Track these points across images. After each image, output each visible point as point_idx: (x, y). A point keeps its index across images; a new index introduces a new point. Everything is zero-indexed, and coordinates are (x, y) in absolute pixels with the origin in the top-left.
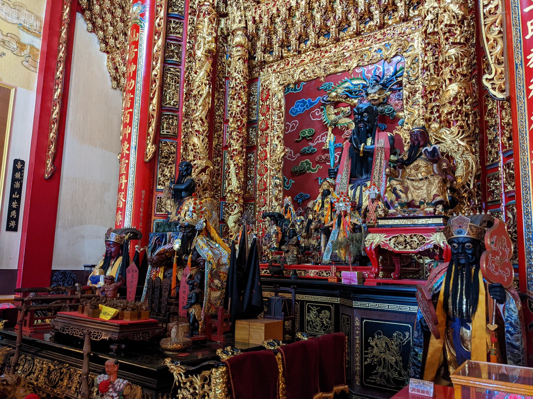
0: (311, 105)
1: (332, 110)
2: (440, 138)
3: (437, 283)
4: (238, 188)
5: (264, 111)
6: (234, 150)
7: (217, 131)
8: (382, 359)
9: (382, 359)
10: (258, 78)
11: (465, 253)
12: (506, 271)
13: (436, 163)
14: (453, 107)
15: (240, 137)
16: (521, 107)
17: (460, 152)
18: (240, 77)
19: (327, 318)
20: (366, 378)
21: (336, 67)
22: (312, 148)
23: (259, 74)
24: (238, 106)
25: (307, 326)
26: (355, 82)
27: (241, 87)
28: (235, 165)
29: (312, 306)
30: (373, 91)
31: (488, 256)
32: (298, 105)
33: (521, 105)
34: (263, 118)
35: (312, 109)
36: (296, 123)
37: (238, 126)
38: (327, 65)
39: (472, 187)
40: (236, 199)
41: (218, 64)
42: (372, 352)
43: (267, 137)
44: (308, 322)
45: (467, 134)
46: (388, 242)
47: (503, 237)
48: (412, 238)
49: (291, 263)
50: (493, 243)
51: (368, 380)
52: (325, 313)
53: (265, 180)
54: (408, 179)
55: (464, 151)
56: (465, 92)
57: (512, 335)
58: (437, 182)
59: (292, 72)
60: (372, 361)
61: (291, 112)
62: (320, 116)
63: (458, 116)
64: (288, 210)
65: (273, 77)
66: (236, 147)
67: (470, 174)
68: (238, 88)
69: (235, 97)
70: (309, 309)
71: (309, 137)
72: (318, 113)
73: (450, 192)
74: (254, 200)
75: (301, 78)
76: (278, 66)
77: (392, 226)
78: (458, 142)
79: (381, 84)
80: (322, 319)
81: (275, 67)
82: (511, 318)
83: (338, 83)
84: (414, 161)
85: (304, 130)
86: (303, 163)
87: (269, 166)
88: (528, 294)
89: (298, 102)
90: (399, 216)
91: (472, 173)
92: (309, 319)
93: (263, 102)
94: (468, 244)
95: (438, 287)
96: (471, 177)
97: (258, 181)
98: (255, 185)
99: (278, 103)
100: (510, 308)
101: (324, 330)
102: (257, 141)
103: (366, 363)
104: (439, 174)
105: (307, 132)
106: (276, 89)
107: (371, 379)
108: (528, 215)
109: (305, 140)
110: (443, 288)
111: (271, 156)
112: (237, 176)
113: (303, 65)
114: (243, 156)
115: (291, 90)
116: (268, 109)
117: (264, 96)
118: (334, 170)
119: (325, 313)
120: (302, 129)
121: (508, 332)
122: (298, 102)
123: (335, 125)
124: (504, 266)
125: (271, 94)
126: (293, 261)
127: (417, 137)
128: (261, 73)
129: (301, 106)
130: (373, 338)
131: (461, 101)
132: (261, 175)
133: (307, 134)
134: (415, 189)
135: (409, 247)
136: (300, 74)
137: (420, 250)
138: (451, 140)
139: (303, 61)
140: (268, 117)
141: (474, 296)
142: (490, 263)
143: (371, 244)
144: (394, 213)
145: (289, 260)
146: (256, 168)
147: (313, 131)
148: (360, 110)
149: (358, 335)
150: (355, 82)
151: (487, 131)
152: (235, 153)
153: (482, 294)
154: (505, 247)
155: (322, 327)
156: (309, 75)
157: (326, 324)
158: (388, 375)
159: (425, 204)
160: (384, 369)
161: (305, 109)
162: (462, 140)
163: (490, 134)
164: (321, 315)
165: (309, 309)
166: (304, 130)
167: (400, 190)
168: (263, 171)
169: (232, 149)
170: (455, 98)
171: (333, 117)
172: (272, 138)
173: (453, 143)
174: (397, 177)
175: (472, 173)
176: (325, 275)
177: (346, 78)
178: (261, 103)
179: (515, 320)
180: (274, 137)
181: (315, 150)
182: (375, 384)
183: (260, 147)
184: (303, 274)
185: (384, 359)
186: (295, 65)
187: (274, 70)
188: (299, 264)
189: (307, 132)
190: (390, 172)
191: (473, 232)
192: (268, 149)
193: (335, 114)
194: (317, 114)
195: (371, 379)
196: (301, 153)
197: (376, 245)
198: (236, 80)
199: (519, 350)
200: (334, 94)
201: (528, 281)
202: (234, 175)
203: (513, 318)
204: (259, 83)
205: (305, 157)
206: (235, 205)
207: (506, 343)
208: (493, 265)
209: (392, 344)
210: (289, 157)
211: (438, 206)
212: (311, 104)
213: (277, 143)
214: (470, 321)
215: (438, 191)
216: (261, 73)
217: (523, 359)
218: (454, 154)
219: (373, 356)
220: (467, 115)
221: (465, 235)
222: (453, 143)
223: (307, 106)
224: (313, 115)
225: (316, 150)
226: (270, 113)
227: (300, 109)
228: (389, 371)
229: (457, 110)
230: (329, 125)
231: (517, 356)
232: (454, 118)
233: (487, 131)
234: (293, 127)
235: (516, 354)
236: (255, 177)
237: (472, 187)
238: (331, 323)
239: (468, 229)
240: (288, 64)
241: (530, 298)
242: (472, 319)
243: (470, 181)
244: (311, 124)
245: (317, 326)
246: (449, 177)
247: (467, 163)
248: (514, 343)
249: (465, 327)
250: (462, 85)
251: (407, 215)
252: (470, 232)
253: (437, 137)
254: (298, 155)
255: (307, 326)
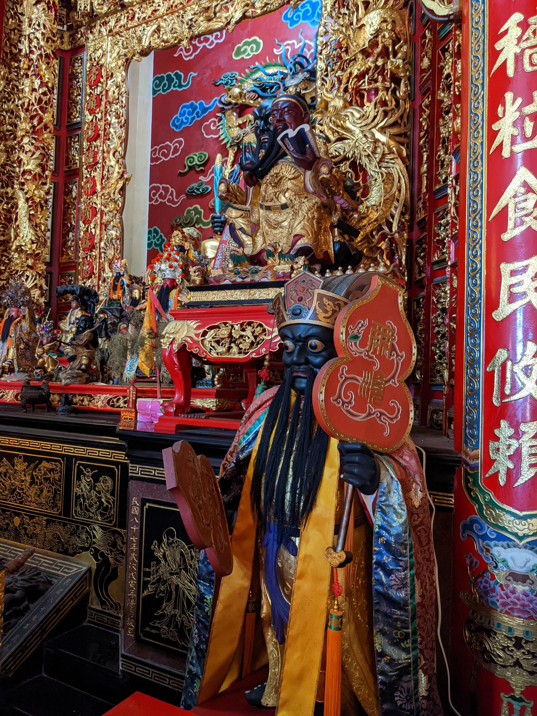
0: (203, 112)
1: (233, 119)
2: (343, 127)
3: (248, 434)
4: (33, 243)
5: (93, 105)
6: (24, 173)
7: (6, 140)
8: (173, 588)
9: (173, 588)
10: (84, 46)
11: (307, 362)
12: (391, 410)
13: (310, 169)
14: (370, 62)
15: (37, 148)
16: (477, 23)
17: (377, 156)
18: (39, 35)
19: (108, 491)
20: (143, 627)
21: (209, 20)
22: (204, 186)
23: (87, 39)
24: (34, 90)
25: (76, 506)
26: (270, 71)
27: (41, 55)
28: (27, 200)
29: (85, 466)
30: (294, 82)
31: (337, 370)
32: (185, 112)
33: (476, 19)
34: (90, 118)
35: (206, 119)
36: (180, 143)
37: (34, 127)
38: (196, 17)
39: (395, 228)
40: (30, 262)
41: (9, 15)
42: (157, 571)
43: (96, 153)
44: (78, 497)
45: (392, 120)
46: (200, 339)
47: (390, 323)
48: (244, 330)
49: (68, 381)
50: (356, 337)
51: (147, 629)
52: (105, 481)
53: (93, 231)
54: (261, 206)
55: (384, 155)
56: (393, 30)
57: (388, 573)
58: (305, 208)
59: (139, 33)
60: (156, 591)
61: (174, 124)
62: (217, 132)
63: (376, 81)
64: (119, 284)
65: (107, 44)
66: (29, 167)
67: (395, 203)
68: (34, 57)
69: (30, 73)
70: (80, 472)
71: (199, 166)
72: (214, 126)
73: (340, 234)
74: (75, 267)
75: (153, 44)
76: (117, 22)
77: (212, 304)
78: (373, 135)
79: (308, 71)
80: (99, 492)
81: (112, 23)
82: (388, 531)
83: (245, 73)
84: (272, 166)
85: (191, 155)
86: (189, 211)
87: (99, 206)
88: (464, 456)
89: (185, 107)
90: (227, 282)
91: (398, 201)
92: (79, 492)
93: (91, 88)
94: (313, 342)
95: (249, 443)
96: (396, 208)
97: (82, 233)
98: (76, 240)
99: (117, 91)
100: (388, 506)
101: (102, 515)
102: (81, 159)
103: (146, 593)
104: (314, 193)
105: (196, 158)
106: (114, 65)
107: (152, 627)
108: (474, 277)
109: (193, 171)
110: (256, 446)
111: (102, 188)
112: (30, 220)
113: (157, 19)
114: (44, 184)
115: (174, 86)
116: (99, 101)
117: (93, 78)
118: (220, 218)
119: (105, 481)
120: (189, 153)
121: (381, 565)
122: (185, 107)
123: (238, 144)
124: (381, 398)
125: (104, 73)
126: (73, 377)
127: (281, 115)
128: (91, 36)
129: (189, 114)
130: (160, 541)
131: (385, 48)
132: (87, 222)
133: (196, 162)
134: (270, 226)
135: (235, 349)
136: (152, 35)
137: (254, 355)
138: (358, 131)
139: (155, 11)
140: (99, 116)
141: (313, 470)
142: (340, 389)
143: (171, 343)
144: (220, 276)
145: (64, 375)
146: (79, 209)
147: (205, 156)
148: (264, 111)
149: (134, 535)
150: (270, 71)
151: (441, 120)
152: (29, 177)
153: (332, 466)
154: (393, 348)
155: (99, 508)
156: (165, 38)
157: (105, 504)
158: (182, 621)
159: (277, 255)
160: (175, 608)
161: (194, 118)
162: (382, 130)
163: (445, 125)
164: (100, 485)
165: (80, 473)
166: (191, 155)
167: (241, 229)
168: (89, 215)
169: (22, 169)
170: (374, 44)
171: (236, 132)
172: (105, 155)
173: (365, 136)
174: (245, 203)
175: (398, 201)
176: (122, 405)
177: (257, 63)
178: (89, 91)
179: (398, 536)
180: (108, 152)
181: (207, 189)
182: (157, 637)
183: (85, 172)
184: (86, 403)
185: (177, 586)
186: (144, 18)
187: (110, 31)
188: (88, 381)
189: (196, 158)
190: (228, 190)
191: (326, 312)
192: (97, 175)
193: (239, 126)
194: (212, 128)
195: (152, 627)
196: (187, 195)
197: (179, 344)
198: (30, 41)
199: (406, 611)
200: (237, 91)
201: (466, 426)
202: (26, 219)
203: (394, 532)
204: (85, 56)
205: (193, 200)
206: (28, 273)
207: (374, 592)
208: (351, 394)
209: (192, 557)
210: (169, 200)
211: (296, 260)
212: (205, 110)
213: (113, 163)
214: (297, 534)
215: (303, 228)
216: (91, 36)
217: (414, 633)
218: (365, 161)
219: (159, 581)
220: (395, 79)
221: (307, 320)
222: (365, 136)
223: (198, 113)
224: (207, 128)
225: (210, 189)
226: (102, 108)
227: (186, 118)
228: (184, 613)
229: (377, 67)
230: (229, 145)
231: (399, 624)
232: (369, 84)
233: (441, 120)
234: (176, 150)
235: (396, 620)
236: (78, 226)
237: (395, 228)
238: (114, 502)
239: (315, 303)
240: (133, 18)
241: (467, 464)
242: (301, 528)
243: (393, 217)
244: (203, 144)
245: (91, 506)
246: (341, 202)
247: (388, 178)
248: (392, 593)
249: (287, 548)
250: (390, 16)
251: (239, 280)
252: (319, 310)
253: (338, 126)
254: (183, 197)
255: (76, 506)
